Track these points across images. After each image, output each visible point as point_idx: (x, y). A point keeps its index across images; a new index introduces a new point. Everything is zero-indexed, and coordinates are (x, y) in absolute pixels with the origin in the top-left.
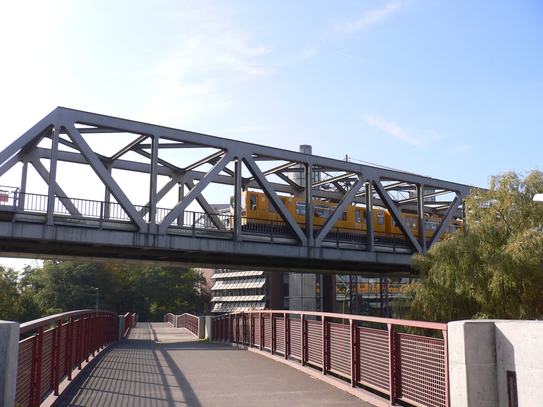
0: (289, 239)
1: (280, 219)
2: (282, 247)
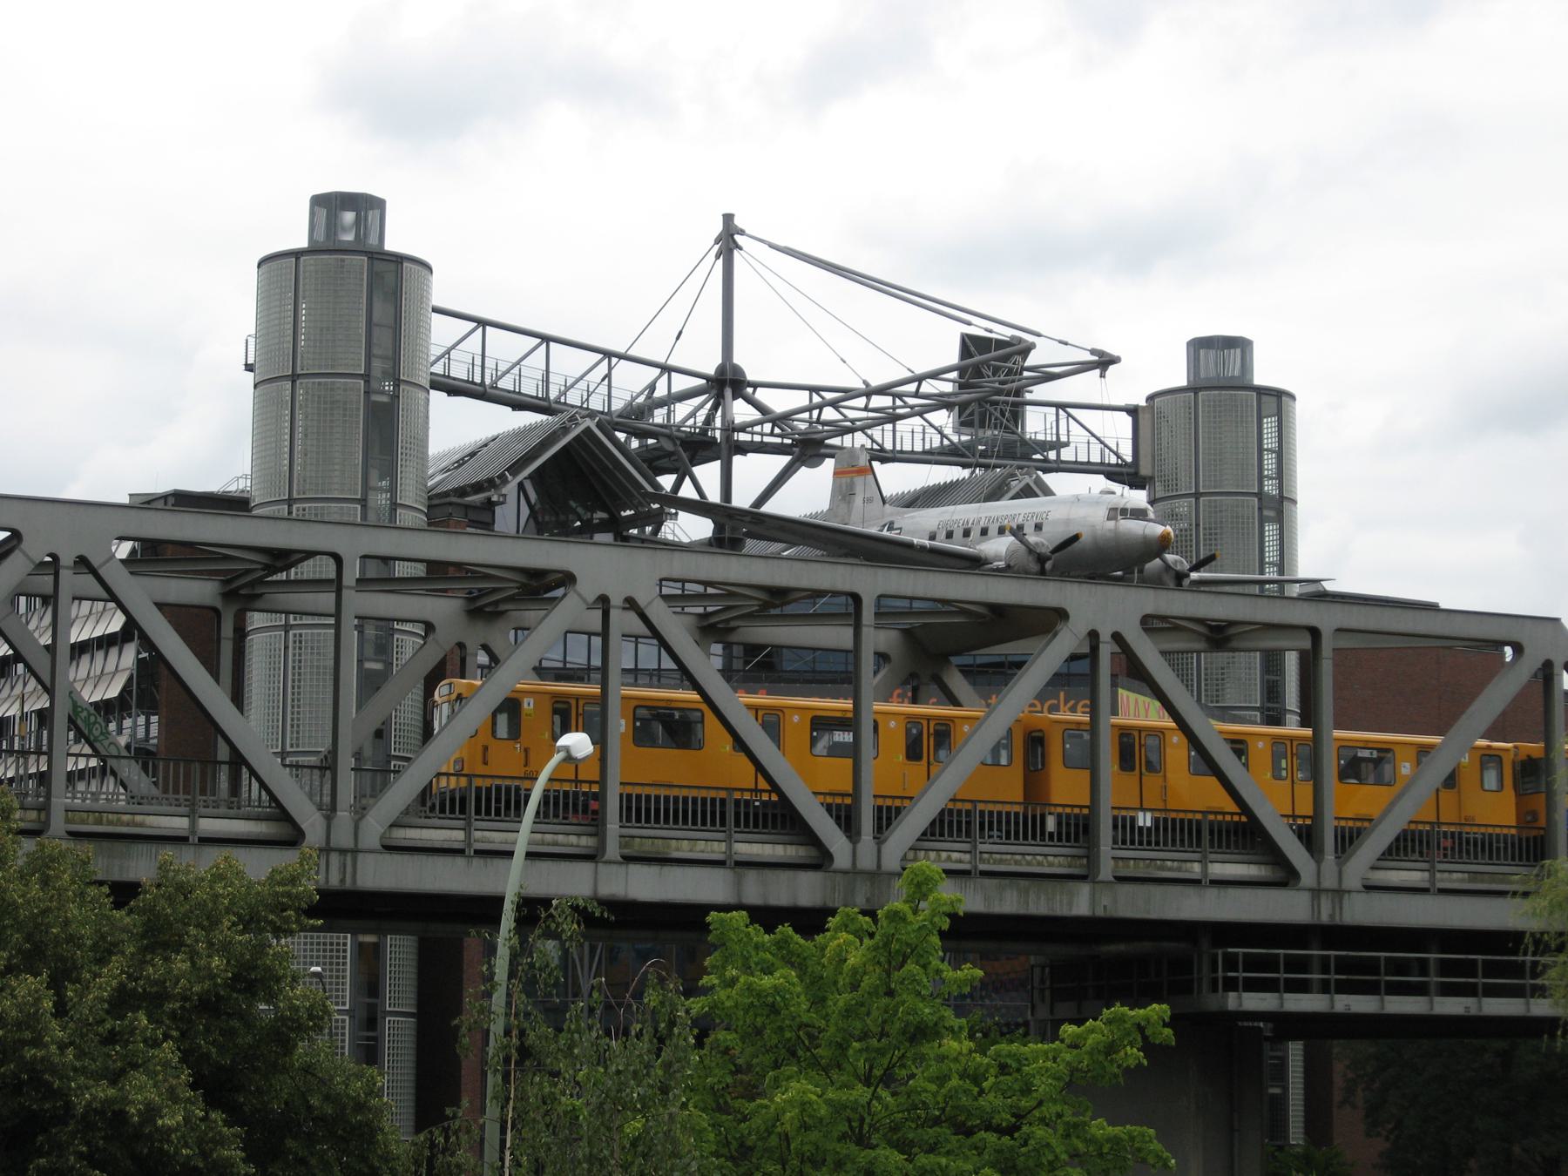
0: (1252, 866)
1: (1231, 806)
2: (1233, 892)
